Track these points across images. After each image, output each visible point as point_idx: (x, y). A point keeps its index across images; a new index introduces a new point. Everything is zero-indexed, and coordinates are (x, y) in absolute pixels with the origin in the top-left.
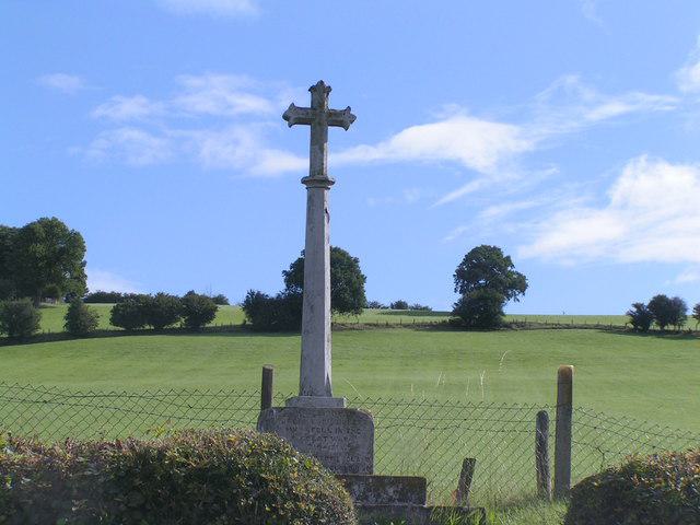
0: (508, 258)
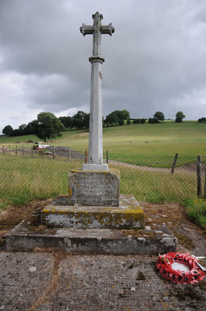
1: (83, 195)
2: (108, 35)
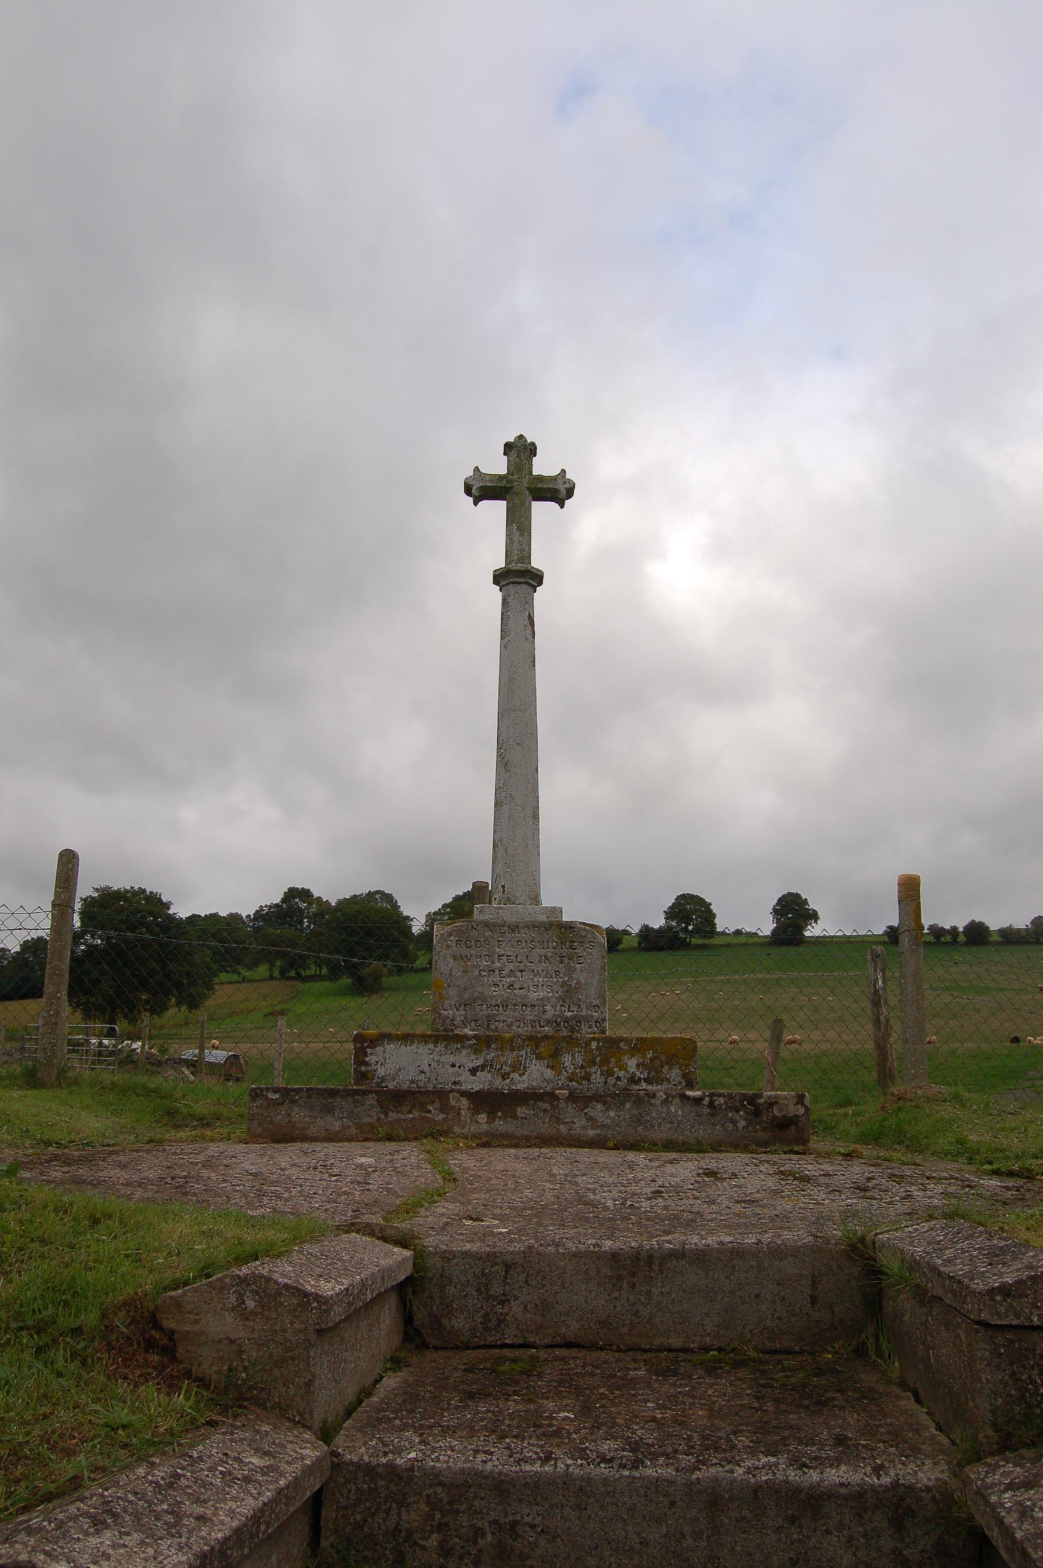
0: (806, 900)
1: (483, 998)
2: (554, 506)
